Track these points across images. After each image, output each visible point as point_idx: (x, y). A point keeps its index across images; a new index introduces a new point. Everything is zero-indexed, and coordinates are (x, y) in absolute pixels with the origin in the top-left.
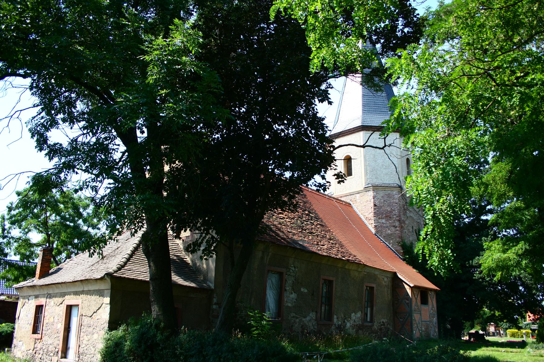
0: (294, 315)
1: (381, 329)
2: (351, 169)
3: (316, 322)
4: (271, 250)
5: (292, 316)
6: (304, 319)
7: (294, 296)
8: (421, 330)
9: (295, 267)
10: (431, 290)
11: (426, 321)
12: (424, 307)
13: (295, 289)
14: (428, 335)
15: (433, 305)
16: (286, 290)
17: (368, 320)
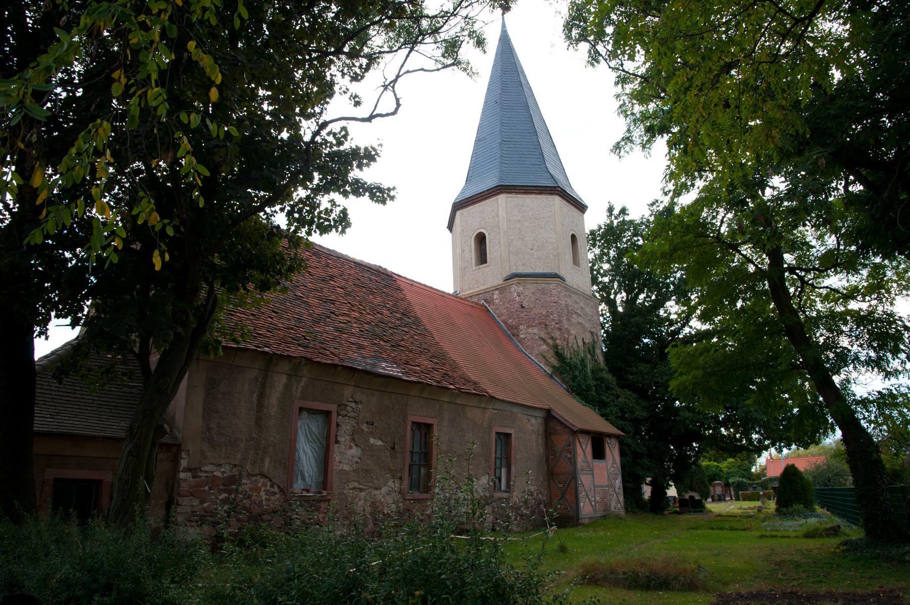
0: (356, 485)
1: (526, 502)
2: (486, 254)
3: (400, 496)
4: (305, 372)
5: (351, 486)
6: (376, 492)
7: (355, 451)
8: (595, 501)
9: (356, 402)
10: (610, 436)
11: (602, 486)
12: (598, 463)
13: (356, 437)
14: (607, 508)
15: (614, 460)
16: (337, 442)
17: (503, 487)
